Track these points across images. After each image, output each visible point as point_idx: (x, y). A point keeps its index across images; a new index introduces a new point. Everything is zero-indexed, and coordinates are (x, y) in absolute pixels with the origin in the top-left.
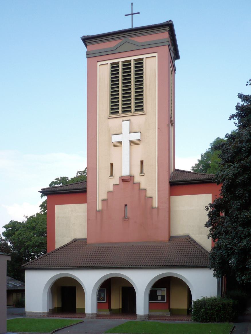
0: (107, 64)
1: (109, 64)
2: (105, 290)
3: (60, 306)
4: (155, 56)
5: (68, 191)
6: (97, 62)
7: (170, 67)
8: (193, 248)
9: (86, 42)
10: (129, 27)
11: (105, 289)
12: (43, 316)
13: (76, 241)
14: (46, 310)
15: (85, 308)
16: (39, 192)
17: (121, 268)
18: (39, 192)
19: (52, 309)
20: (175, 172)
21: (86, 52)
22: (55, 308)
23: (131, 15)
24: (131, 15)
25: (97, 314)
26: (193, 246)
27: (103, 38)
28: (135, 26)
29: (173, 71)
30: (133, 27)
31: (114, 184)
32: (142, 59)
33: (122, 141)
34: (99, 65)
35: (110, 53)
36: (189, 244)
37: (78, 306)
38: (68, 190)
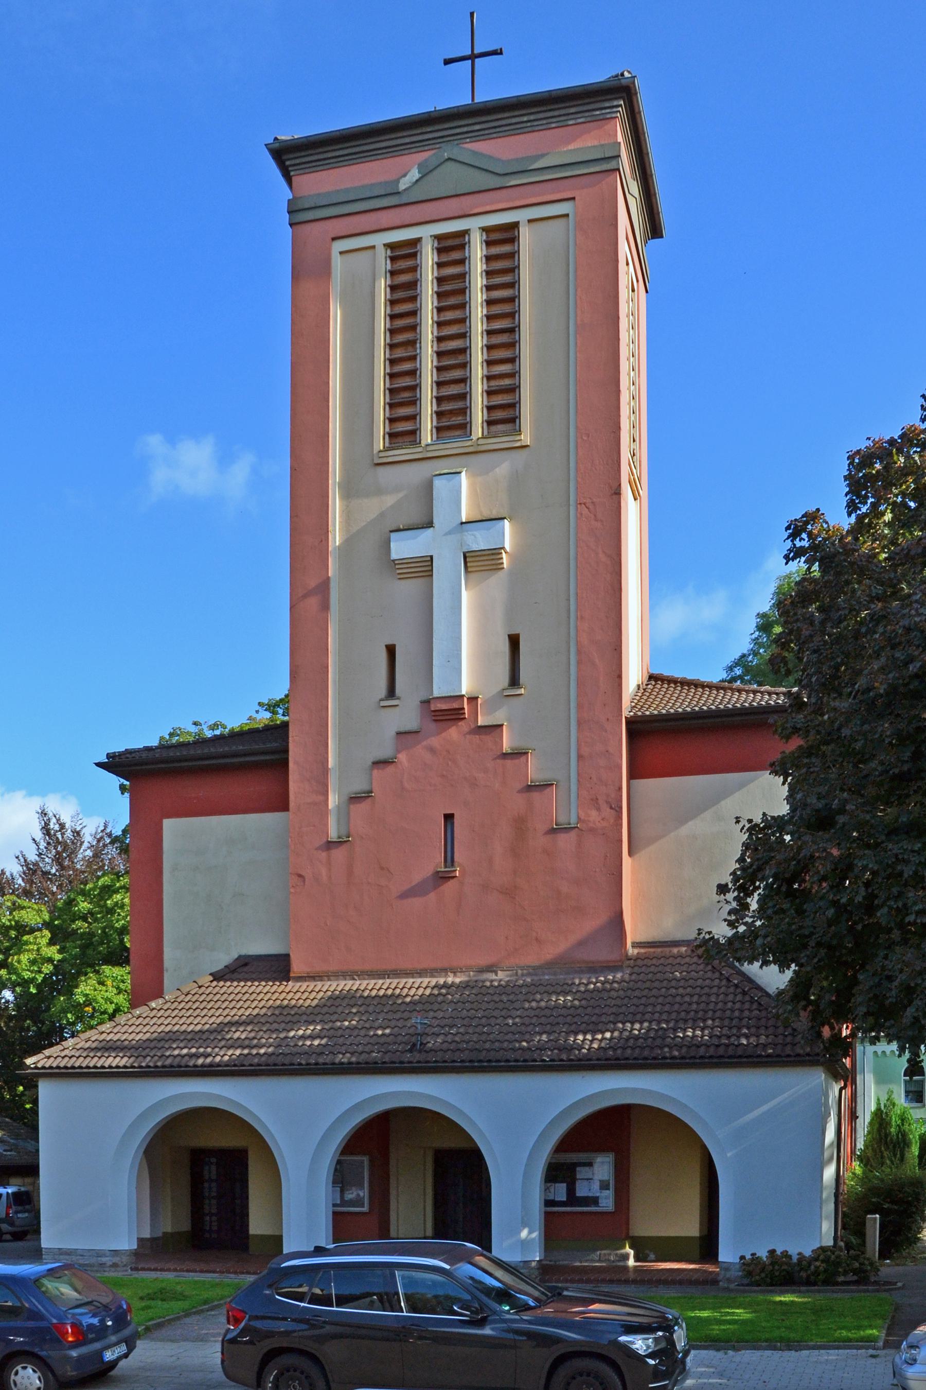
0: (373, 247)
1: (382, 254)
2: (362, 1162)
3: (185, 1226)
4: (567, 215)
5: (248, 759)
6: (334, 239)
7: (628, 264)
8: (723, 990)
9: (288, 163)
10: (463, 99)
11: (366, 1159)
12: (111, 1266)
13: (246, 965)
14: (127, 1243)
15: (282, 1236)
16: (98, 765)
17: (161, 1076)
18: (98, 765)
19: (153, 1240)
20: (649, 686)
21: (289, 200)
22: (164, 1233)
23: (476, 52)
24: (476, 52)
25: (544, 1262)
26: (724, 982)
27: (553, 107)
28: (482, 97)
29: (638, 281)
30: (476, 101)
31: (402, 730)
32: (515, 226)
33: (431, 557)
34: (341, 253)
35: (382, 206)
36: (709, 974)
37: (257, 1225)
38: (186, 760)
